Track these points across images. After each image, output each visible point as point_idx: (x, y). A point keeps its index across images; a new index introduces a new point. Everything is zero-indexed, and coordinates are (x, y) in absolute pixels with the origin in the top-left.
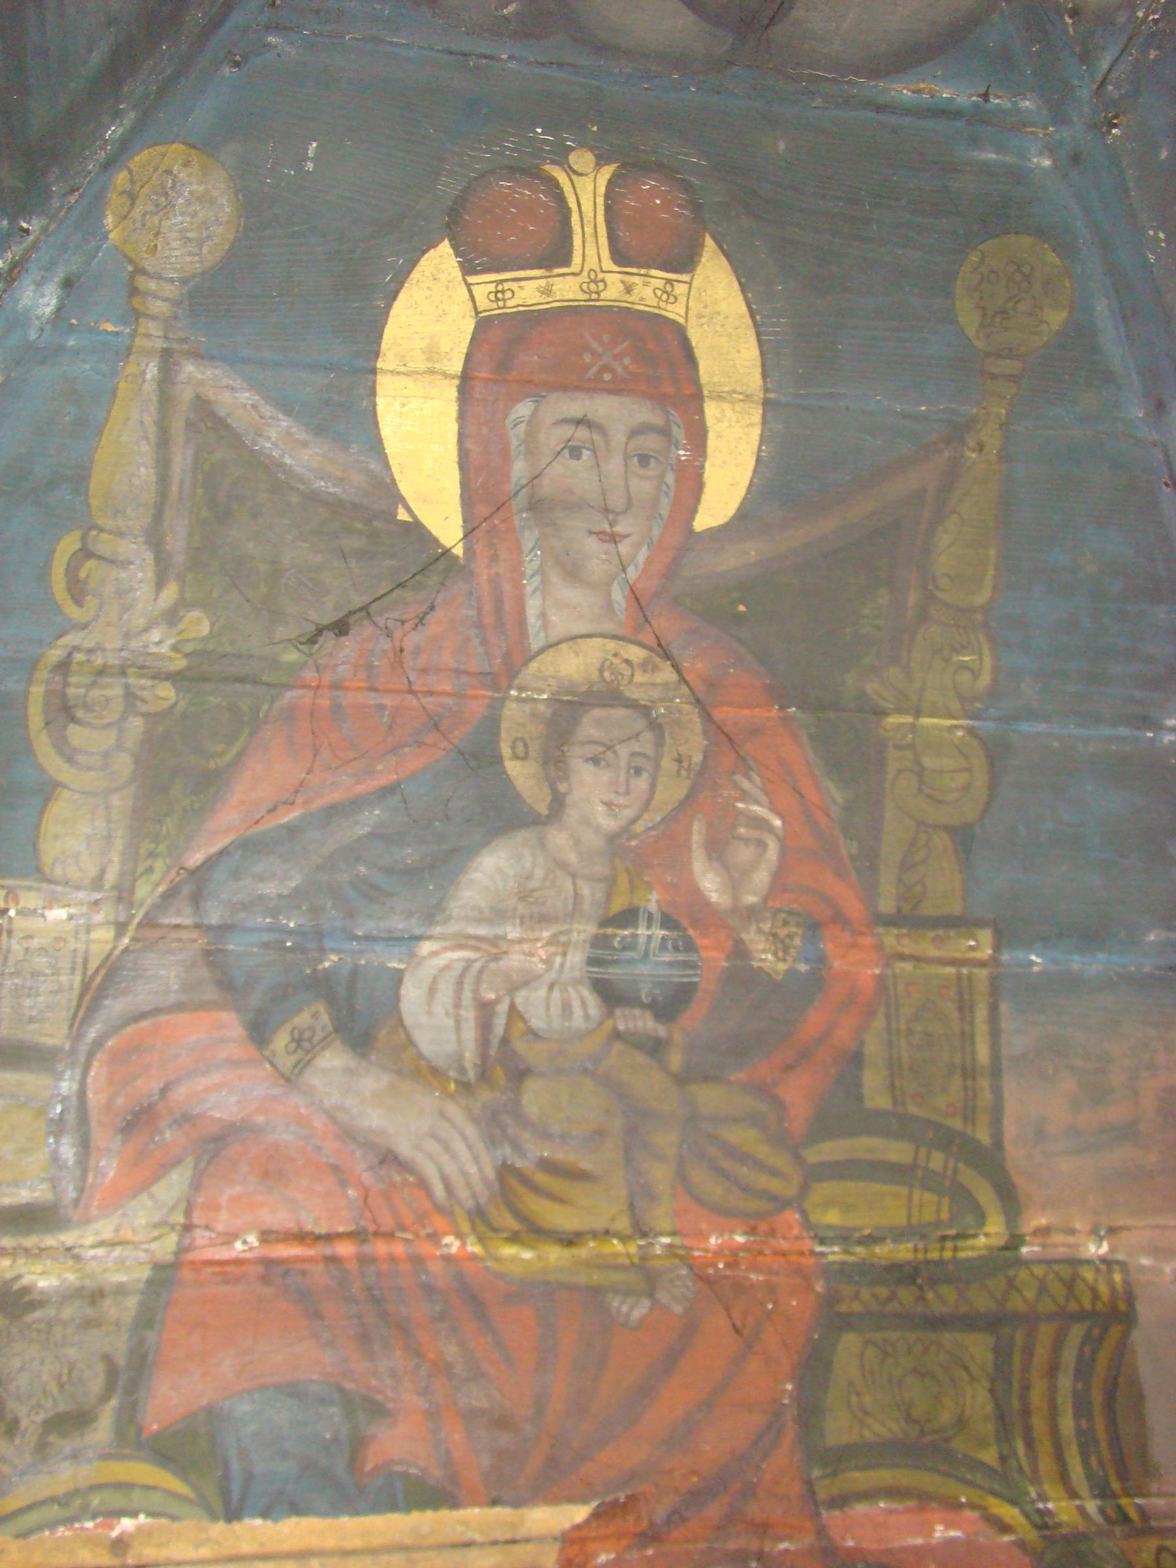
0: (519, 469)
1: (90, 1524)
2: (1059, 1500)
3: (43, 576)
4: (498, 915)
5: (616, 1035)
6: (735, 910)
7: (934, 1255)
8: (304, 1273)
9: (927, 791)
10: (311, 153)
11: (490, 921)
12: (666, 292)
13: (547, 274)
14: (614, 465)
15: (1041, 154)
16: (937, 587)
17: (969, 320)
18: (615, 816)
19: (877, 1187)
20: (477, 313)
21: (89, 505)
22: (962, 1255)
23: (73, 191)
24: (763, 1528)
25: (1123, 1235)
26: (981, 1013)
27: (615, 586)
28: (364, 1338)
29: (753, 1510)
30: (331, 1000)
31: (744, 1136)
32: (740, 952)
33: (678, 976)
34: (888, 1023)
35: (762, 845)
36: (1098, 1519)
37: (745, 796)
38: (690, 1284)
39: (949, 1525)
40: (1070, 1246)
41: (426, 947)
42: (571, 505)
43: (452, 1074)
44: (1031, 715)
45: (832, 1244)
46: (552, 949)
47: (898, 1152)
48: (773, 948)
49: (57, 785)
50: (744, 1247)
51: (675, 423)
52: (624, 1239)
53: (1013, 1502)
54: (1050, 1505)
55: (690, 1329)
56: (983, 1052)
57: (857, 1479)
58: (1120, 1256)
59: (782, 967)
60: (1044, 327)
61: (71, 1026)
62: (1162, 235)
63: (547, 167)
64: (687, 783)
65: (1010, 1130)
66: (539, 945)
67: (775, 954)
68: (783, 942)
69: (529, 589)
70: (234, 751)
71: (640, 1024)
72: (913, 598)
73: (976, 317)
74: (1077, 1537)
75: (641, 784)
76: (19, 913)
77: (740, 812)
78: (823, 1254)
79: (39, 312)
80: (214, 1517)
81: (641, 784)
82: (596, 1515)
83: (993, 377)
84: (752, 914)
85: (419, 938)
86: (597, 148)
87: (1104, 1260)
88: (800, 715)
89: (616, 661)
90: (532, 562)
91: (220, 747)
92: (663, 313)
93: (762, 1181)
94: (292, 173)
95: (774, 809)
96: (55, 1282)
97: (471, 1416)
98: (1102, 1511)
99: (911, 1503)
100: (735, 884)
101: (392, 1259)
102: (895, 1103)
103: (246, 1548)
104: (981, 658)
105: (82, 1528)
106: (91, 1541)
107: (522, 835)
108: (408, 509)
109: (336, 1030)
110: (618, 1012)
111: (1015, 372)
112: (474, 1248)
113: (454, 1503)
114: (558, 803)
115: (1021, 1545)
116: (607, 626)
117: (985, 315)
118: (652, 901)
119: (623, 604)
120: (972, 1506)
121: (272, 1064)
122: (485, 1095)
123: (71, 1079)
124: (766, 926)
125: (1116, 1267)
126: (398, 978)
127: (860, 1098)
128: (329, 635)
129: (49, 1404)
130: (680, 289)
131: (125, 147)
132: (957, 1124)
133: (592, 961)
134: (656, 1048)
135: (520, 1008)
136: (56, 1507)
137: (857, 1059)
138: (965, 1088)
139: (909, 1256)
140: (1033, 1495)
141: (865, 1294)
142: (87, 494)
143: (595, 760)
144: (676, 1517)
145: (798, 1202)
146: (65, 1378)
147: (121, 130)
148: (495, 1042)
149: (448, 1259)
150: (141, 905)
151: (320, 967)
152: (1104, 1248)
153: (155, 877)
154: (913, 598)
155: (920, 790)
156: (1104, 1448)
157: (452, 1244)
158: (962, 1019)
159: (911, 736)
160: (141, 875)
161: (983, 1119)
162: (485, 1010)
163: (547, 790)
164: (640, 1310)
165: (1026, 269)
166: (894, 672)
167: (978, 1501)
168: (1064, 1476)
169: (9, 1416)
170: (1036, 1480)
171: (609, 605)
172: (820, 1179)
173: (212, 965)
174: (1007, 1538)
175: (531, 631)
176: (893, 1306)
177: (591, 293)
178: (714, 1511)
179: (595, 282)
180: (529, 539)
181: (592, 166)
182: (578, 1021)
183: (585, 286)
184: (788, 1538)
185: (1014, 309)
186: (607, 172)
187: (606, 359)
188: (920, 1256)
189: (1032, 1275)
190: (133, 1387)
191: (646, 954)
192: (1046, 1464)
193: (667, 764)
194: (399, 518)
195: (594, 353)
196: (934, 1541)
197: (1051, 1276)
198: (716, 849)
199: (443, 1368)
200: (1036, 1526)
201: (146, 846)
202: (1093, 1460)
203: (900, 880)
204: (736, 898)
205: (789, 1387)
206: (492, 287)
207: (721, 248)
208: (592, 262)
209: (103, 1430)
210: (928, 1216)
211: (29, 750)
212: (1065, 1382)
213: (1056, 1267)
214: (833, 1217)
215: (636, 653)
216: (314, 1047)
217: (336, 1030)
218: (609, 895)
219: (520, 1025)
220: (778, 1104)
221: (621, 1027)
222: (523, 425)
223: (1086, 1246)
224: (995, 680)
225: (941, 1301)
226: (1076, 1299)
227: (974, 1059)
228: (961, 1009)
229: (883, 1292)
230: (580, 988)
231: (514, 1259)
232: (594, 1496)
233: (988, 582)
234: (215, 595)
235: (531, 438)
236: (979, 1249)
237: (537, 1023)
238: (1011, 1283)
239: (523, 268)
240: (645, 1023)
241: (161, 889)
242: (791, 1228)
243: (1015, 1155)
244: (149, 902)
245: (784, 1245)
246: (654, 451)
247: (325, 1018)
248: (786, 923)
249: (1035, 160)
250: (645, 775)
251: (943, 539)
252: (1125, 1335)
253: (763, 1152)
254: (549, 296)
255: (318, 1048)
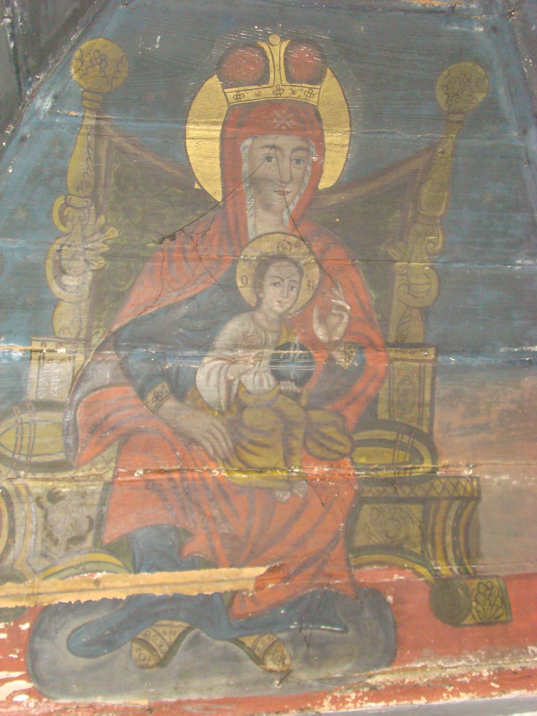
0: (245, 167)
1: (86, 575)
2: (442, 566)
3: (49, 214)
4: (235, 346)
5: (280, 392)
6: (330, 342)
7: (402, 475)
8: (161, 485)
9: (411, 293)
10: (158, 41)
11: (232, 350)
12: (309, 93)
13: (258, 87)
14: (286, 164)
15: (478, 26)
16: (421, 209)
17: (441, 98)
18: (283, 306)
19: (381, 449)
20: (228, 104)
21: (67, 186)
22: (413, 475)
23: (57, 61)
24: (330, 576)
25: (479, 467)
26: (428, 381)
27: (285, 213)
28: (183, 508)
29: (327, 569)
30: (169, 382)
31: (331, 431)
32: (331, 359)
33: (305, 368)
34: (390, 385)
35: (341, 316)
36: (457, 573)
37: (336, 297)
38: (306, 486)
39: (399, 575)
40: (456, 471)
41: (206, 360)
42: (267, 180)
43: (216, 408)
44: (458, 261)
45: (361, 471)
46: (256, 359)
47: (390, 435)
48: (344, 356)
49: (59, 300)
50: (328, 472)
51: (312, 146)
52: (282, 470)
53: (425, 566)
54: (439, 568)
55: (306, 502)
56: (427, 396)
57: (366, 558)
58: (477, 475)
59: (348, 364)
60: (475, 101)
61: (69, 394)
62: (531, 61)
63: (259, 43)
64: (312, 292)
65: (436, 427)
66: (251, 358)
67: (345, 359)
68: (348, 354)
69: (249, 215)
70: (129, 284)
71: (290, 388)
72: (410, 214)
73: (445, 97)
74: (448, 579)
75: (293, 293)
76: (47, 351)
77: (334, 304)
78: (357, 475)
79: (44, 108)
80: (130, 572)
81: (293, 293)
82: (268, 571)
83: (451, 122)
84: (336, 344)
85: (203, 356)
86: (281, 34)
87: (470, 477)
88: (360, 263)
89: (284, 243)
90: (250, 203)
91: (124, 283)
92: (308, 101)
93: (336, 447)
94: (150, 49)
95: (347, 302)
96: (68, 490)
97: (223, 536)
98: (459, 570)
99: (386, 567)
100: (329, 333)
101: (194, 479)
102: (390, 417)
103: (142, 582)
104: (438, 238)
105: (84, 577)
106: (88, 581)
107: (244, 316)
108: (199, 184)
109: (171, 392)
110: (281, 383)
111: (460, 120)
112: (224, 474)
113: (216, 566)
114: (259, 302)
115: (427, 582)
116: (281, 229)
117: (449, 97)
118: (297, 340)
119: (288, 220)
120: (409, 568)
121: (147, 406)
122: (229, 416)
123: (71, 414)
124: (342, 348)
125: (475, 479)
126: (195, 372)
127: (376, 415)
128: (167, 241)
129: (69, 533)
130: (316, 91)
131: (79, 41)
132: (415, 424)
133: (272, 363)
134: (296, 397)
135: (243, 382)
136: (74, 569)
137: (375, 400)
138: (419, 412)
139: (392, 475)
140: (433, 564)
141: (374, 490)
142: (66, 182)
143: (275, 284)
144: (298, 572)
145: (349, 455)
146: (74, 524)
147: (77, 36)
148: (233, 396)
149: (214, 478)
150: (94, 346)
151: (165, 368)
152: (471, 472)
153: (99, 335)
154: (410, 214)
155: (408, 293)
156: (462, 548)
157: (216, 473)
158: (420, 383)
159: (406, 270)
160: (94, 335)
161: (425, 422)
162: (229, 383)
163: (255, 297)
164: (287, 496)
165: (468, 76)
166: (401, 244)
167: (411, 566)
168: (446, 558)
169: (55, 538)
170: (435, 559)
171: (282, 221)
172: (358, 446)
173: (123, 368)
174: (421, 579)
175: (249, 231)
176: (385, 494)
177: (277, 94)
178: (311, 570)
179: (279, 90)
180: (249, 194)
181: (279, 42)
182: (266, 386)
183: (275, 92)
184: (340, 578)
185: (462, 93)
186: (285, 44)
187: (283, 121)
188: (397, 475)
189: (441, 482)
190: (99, 527)
191: (293, 360)
192: (439, 553)
193: (304, 284)
194: (195, 187)
195: (279, 119)
196: (394, 580)
197: (448, 483)
198: (323, 319)
199: (213, 519)
200: (433, 576)
201: (96, 323)
202: (458, 553)
203: (397, 330)
204: (330, 337)
205: (342, 525)
206: (235, 94)
207: (334, 74)
208: (278, 82)
209: (89, 542)
210: (401, 460)
211: (48, 286)
212: (450, 523)
213: (451, 479)
214: (363, 460)
215: (293, 240)
216: (163, 399)
217: (171, 392)
218: (279, 337)
219: (243, 389)
220: (344, 419)
221: (283, 389)
222: (247, 149)
223: (463, 472)
224: (444, 246)
225: (404, 492)
226: (458, 492)
227: (423, 399)
228: (420, 380)
229: (381, 489)
230: (266, 374)
231: (239, 479)
232: (268, 564)
233: (443, 207)
234: (120, 220)
235: (250, 153)
236: (420, 472)
237: (249, 387)
238: (432, 485)
239: (248, 85)
240: (292, 387)
241: (102, 340)
242: (346, 465)
243: (437, 436)
244: (97, 345)
245: (343, 471)
246: (303, 158)
247: (167, 388)
248: (350, 347)
249: (476, 29)
250: (295, 289)
251: (425, 190)
252: (476, 505)
253: (337, 436)
254: (259, 96)
255: (165, 400)
